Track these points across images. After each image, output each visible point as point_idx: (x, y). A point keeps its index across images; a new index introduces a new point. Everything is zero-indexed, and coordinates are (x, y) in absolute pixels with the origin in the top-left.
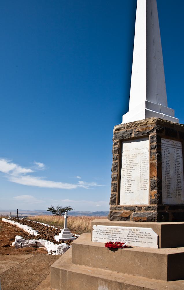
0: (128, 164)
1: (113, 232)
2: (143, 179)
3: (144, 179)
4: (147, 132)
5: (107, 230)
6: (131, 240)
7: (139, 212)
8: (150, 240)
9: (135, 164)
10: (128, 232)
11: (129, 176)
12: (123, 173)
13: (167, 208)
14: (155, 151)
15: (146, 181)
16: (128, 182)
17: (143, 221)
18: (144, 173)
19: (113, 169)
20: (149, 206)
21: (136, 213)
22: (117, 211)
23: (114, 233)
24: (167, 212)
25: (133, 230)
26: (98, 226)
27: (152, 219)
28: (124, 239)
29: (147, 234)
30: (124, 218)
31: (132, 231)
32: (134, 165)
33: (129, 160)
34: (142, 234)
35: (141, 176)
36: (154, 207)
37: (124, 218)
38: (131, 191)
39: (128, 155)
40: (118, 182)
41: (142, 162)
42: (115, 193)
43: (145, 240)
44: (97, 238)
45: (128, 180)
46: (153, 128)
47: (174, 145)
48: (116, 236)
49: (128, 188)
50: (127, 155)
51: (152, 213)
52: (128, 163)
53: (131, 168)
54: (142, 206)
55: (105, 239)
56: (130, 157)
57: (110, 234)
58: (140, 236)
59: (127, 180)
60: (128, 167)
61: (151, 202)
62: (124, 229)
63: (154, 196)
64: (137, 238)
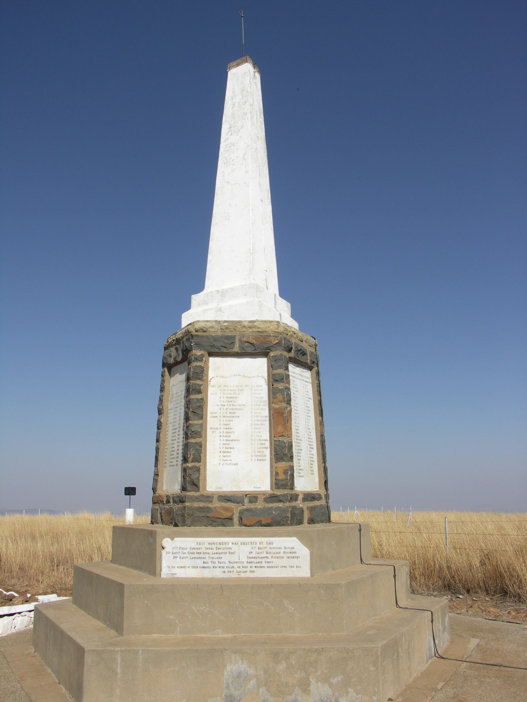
0: (223, 404)
2: (256, 438)
5: (198, 546)
6: (256, 565)
8: (295, 562)
9: (239, 405)
10: (248, 548)
11: (228, 430)
13: (301, 497)
15: (263, 442)
16: (225, 442)
18: (258, 426)
21: (245, 507)
23: (217, 553)
25: (260, 543)
26: (175, 539)
28: (241, 565)
29: (289, 550)
31: (258, 545)
32: (238, 407)
33: (227, 397)
34: (279, 551)
35: (252, 432)
38: (233, 462)
39: (224, 386)
43: (284, 562)
44: (173, 567)
52: (223, 401)
53: (230, 413)
54: (259, 494)
55: (194, 567)
56: (228, 390)
57: (207, 556)
58: (274, 555)
59: (222, 438)
60: (225, 411)
62: (240, 544)
64: (267, 560)
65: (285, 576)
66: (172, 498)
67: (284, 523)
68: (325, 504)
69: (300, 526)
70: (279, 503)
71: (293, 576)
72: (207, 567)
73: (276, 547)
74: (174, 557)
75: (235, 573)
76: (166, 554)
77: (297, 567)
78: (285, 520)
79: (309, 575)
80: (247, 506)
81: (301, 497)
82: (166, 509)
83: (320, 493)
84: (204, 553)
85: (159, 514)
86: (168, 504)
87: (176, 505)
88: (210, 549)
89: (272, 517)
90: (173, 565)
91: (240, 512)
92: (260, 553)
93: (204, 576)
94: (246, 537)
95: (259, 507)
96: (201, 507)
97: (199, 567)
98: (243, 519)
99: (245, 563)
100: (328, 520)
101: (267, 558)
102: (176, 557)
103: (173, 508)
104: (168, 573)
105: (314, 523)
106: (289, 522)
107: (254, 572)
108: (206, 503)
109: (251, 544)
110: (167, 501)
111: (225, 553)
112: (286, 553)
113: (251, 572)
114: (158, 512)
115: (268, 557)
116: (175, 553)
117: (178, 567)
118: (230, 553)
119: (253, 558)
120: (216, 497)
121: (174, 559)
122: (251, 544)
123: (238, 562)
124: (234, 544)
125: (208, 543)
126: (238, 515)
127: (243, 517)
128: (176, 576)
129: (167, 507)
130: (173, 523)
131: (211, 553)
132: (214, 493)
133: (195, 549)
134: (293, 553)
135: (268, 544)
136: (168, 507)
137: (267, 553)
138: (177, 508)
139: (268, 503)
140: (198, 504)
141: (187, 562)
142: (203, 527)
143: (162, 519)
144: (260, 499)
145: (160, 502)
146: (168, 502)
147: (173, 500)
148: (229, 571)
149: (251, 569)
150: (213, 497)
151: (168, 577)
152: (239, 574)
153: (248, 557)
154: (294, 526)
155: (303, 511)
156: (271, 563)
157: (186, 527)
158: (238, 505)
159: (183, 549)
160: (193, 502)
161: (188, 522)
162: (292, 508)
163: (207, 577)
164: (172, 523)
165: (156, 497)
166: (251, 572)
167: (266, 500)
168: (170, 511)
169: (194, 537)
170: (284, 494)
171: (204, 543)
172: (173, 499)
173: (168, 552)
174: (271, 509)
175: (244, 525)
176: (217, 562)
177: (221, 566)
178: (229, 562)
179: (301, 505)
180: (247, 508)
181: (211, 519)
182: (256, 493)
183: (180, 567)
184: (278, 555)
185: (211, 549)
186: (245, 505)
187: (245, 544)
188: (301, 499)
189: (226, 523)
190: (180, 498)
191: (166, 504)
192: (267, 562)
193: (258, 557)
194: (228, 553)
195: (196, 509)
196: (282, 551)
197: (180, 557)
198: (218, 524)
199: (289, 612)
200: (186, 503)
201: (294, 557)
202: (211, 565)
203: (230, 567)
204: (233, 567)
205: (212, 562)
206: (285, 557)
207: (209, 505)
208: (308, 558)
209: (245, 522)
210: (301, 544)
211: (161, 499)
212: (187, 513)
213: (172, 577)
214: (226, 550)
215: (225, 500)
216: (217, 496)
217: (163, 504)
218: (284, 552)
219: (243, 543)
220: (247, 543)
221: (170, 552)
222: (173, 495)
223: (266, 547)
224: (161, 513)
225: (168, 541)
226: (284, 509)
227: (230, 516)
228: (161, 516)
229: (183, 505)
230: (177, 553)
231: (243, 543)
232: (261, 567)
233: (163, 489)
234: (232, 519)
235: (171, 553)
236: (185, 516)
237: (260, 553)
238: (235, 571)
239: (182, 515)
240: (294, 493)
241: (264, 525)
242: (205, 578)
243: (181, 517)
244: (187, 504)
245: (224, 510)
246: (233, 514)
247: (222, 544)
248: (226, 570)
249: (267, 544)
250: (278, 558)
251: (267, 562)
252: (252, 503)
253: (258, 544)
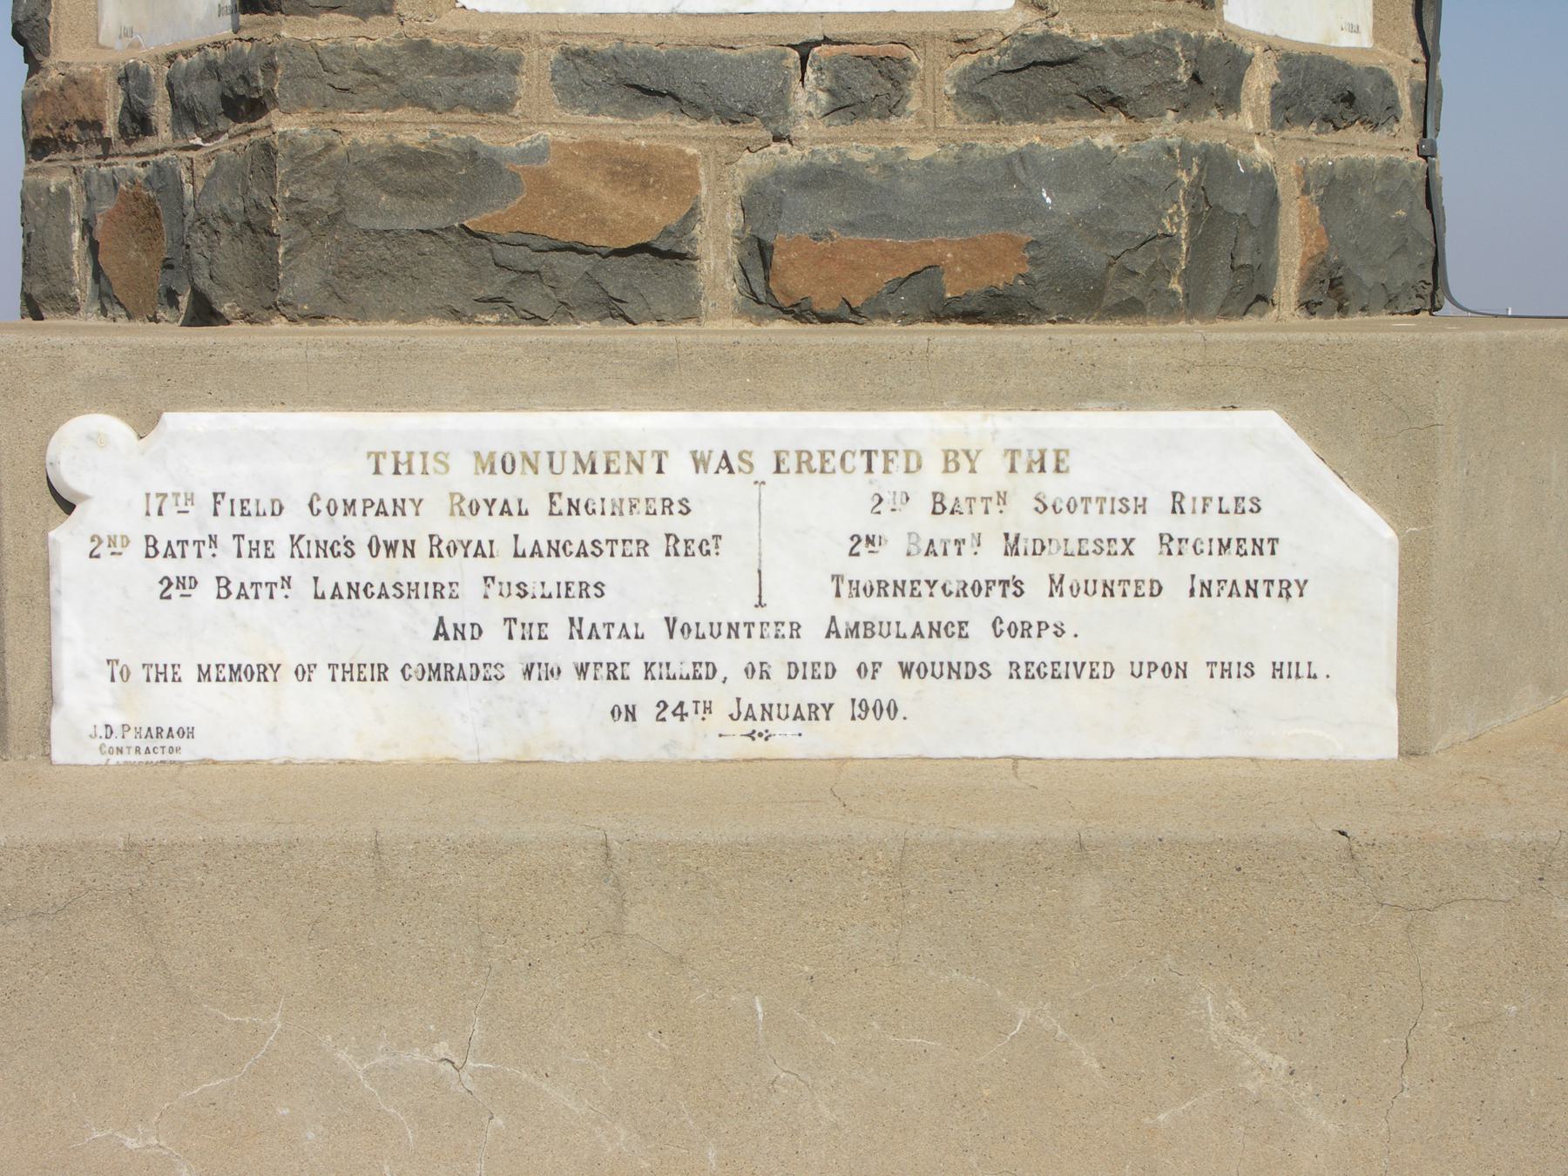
1: (538, 528)
5: (388, 488)
6: (915, 651)
13: (1260, 80)
21: (794, 156)
23: (557, 549)
25: (951, 461)
26: (175, 421)
28: (776, 653)
29: (1215, 526)
31: (933, 477)
34: (1119, 526)
44: (163, 674)
55: (349, 672)
58: (1075, 569)
62: (764, 465)
64: (1013, 610)
65: (1166, 751)
66: (163, 90)
67: (1131, 288)
68: (1415, 159)
69: (1251, 321)
70: (1096, 122)
71: (1246, 752)
72: (468, 671)
73: (1094, 494)
74: (167, 582)
75: (719, 719)
76: (93, 555)
77: (1277, 670)
78: (1141, 262)
79: (1382, 743)
80: (814, 141)
81: (1260, 80)
82: (122, 186)
83: (1390, 71)
84: (437, 547)
85: (77, 234)
86: (140, 147)
87: (198, 141)
88: (497, 509)
89: (1028, 237)
90: (163, 657)
91: (751, 191)
92: (952, 549)
93: (440, 750)
94: (823, 401)
95: (921, 152)
96: (414, 151)
97: (394, 674)
98: (777, 260)
99: (814, 630)
100: (1429, 289)
101: (1012, 589)
102: (181, 582)
103: (173, 171)
104: (116, 720)
105: (1342, 309)
106: (1175, 286)
107: (892, 710)
108: (456, 117)
109: (869, 469)
110: (127, 122)
111: (632, 548)
112: (1188, 548)
113: (862, 709)
114: (66, 217)
115: (1018, 583)
116: (178, 550)
117: (204, 674)
118: (674, 546)
119: (880, 588)
120: (538, 61)
121: (165, 596)
122: (869, 469)
123: (749, 625)
124: (713, 465)
125: (478, 455)
126: (732, 219)
127: (778, 239)
128: (189, 751)
129: (128, 166)
130: (184, 301)
131: (504, 547)
132: (520, 28)
133: (359, 507)
134: (1249, 546)
135: (1021, 466)
136: (141, 170)
137: (1012, 547)
138: (204, 171)
139: (996, 116)
140: (381, 123)
142: (433, 325)
143: (98, 274)
144: (929, 84)
145: (74, 133)
146: (138, 123)
147: (174, 106)
148: (672, 706)
149: (870, 691)
150: (513, 65)
151: (115, 759)
152: (760, 726)
153: (837, 578)
154: (1213, 318)
155: (1273, 201)
156: (1048, 634)
157: (280, 324)
158: (738, 133)
159: (251, 507)
160: (337, 109)
161: (301, 281)
162: (1201, 170)
163: (472, 758)
164: (171, 298)
165: (44, 94)
166: (862, 709)
167: (980, 89)
168: (150, 200)
169: (349, 408)
170: (1136, 40)
171: (442, 459)
172: (172, 95)
173: (112, 542)
174: (1018, 169)
175: (787, 304)
176: (558, 629)
177: (598, 664)
178: (670, 623)
179: (1262, 153)
180: (817, 160)
181: (504, 254)
182: (891, 27)
183: (226, 673)
184: (1109, 568)
185: (505, 511)
186: (795, 133)
187: (816, 463)
188: (1265, 101)
189: (629, 296)
190: (232, 77)
191: (123, 147)
192: (1013, 630)
193: (931, 584)
194: (657, 547)
195: (368, 169)
196: (1145, 530)
197: (223, 583)
198: (562, 296)
199: (1247, 1092)
200: (274, 114)
201: (1252, 589)
202: (513, 654)
203: (674, 669)
204: (705, 671)
205: (517, 630)
206: (1176, 588)
207: (478, 136)
208: (1384, 595)
209: (794, 279)
210: (1324, 471)
211: (85, 111)
212: (294, 200)
213: (153, 758)
214: (640, 518)
215: (617, 93)
216: (553, 53)
217: (99, 151)
218: (1165, 540)
219: (790, 462)
220: (835, 462)
221: (126, 542)
222: (171, 58)
223: (1002, 498)
224: (87, 227)
225: (98, 440)
226: (1137, 171)
227: (667, 232)
228: (94, 248)
229: (253, 137)
230: (191, 551)
231: (790, 462)
232: (953, 671)
233: (103, 28)
234: (682, 256)
235: (139, 546)
236: (277, 224)
237: (952, 549)
238: (724, 706)
239: (248, 224)
240: (1215, 34)
241: (959, 308)
242: (451, 764)
243: (237, 236)
244: (285, 124)
245: (614, 174)
246: (693, 213)
247: (600, 467)
248: (643, 694)
249: (1013, 470)
250: (1108, 589)
251: (1013, 630)
252: (204, 760)
253: (933, 464)
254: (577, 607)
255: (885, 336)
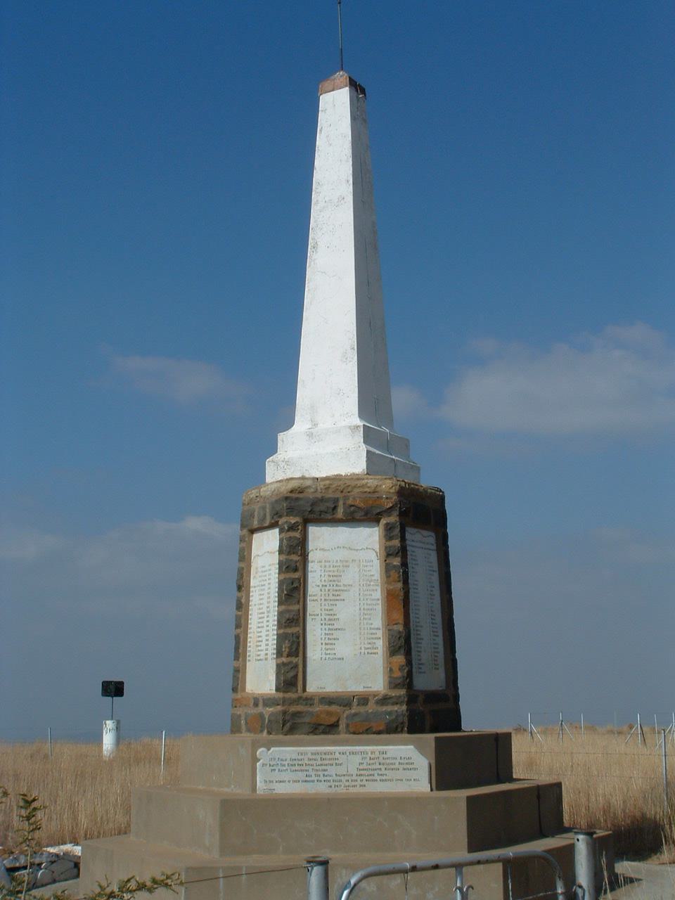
1: (319, 762)
3: (369, 626)
4: (378, 511)
5: (300, 757)
6: (367, 778)
7: (362, 709)
9: (344, 585)
10: (357, 759)
12: (314, 606)
13: (421, 698)
14: (397, 561)
15: (374, 631)
17: (374, 733)
19: (285, 595)
20: (386, 695)
21: (353, 711)
22: (302, 707)
24: (421, 708)
25: (372, 754)
27: (397, 727)
30: (323, 727)
32: (342, 588)
36: (400, 697)
37: (323, 727)
40: (301, 632)
41: (362, 583)
42: (294, 660)
44: (270, 782)
45: (327, 627)
46: (391, 505)
47: (424, 543)
48: (326, 773)
49: (328, 647)
50: (320, 562)
51: (396, 711)
53: (333, 595)
54: (370, 695)
55: (284, 782)
59: (323, 627)
61: (393, 684)
62: (348, 754)
63: (399, 669)
64: (380, 773)
77: (414, 780)
90: (271, 779)
113: (361, 786)
128: (274, 792)
141: (286, 776)
166: (361, 786)
176: (322, 775)
194: (334, 765)
204: (341, 781)
248: (332, 784)
253: (370, 753)
254: (324, 773)
255: (365, 736)
